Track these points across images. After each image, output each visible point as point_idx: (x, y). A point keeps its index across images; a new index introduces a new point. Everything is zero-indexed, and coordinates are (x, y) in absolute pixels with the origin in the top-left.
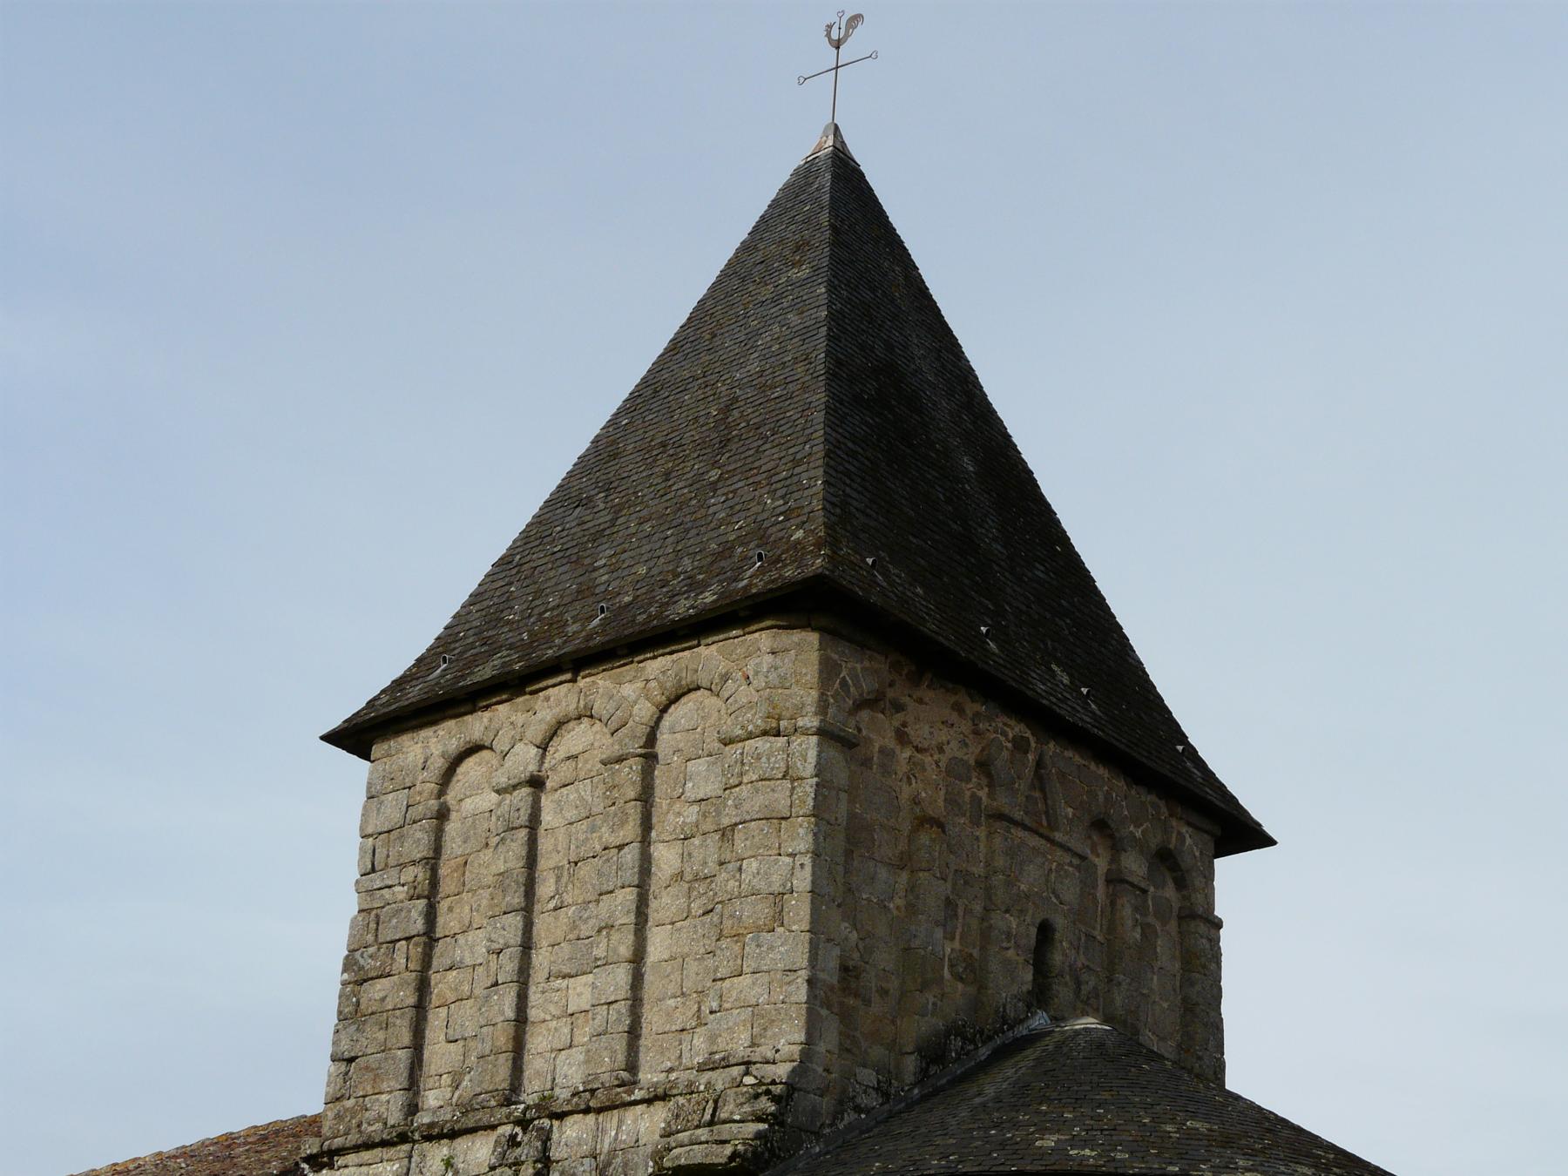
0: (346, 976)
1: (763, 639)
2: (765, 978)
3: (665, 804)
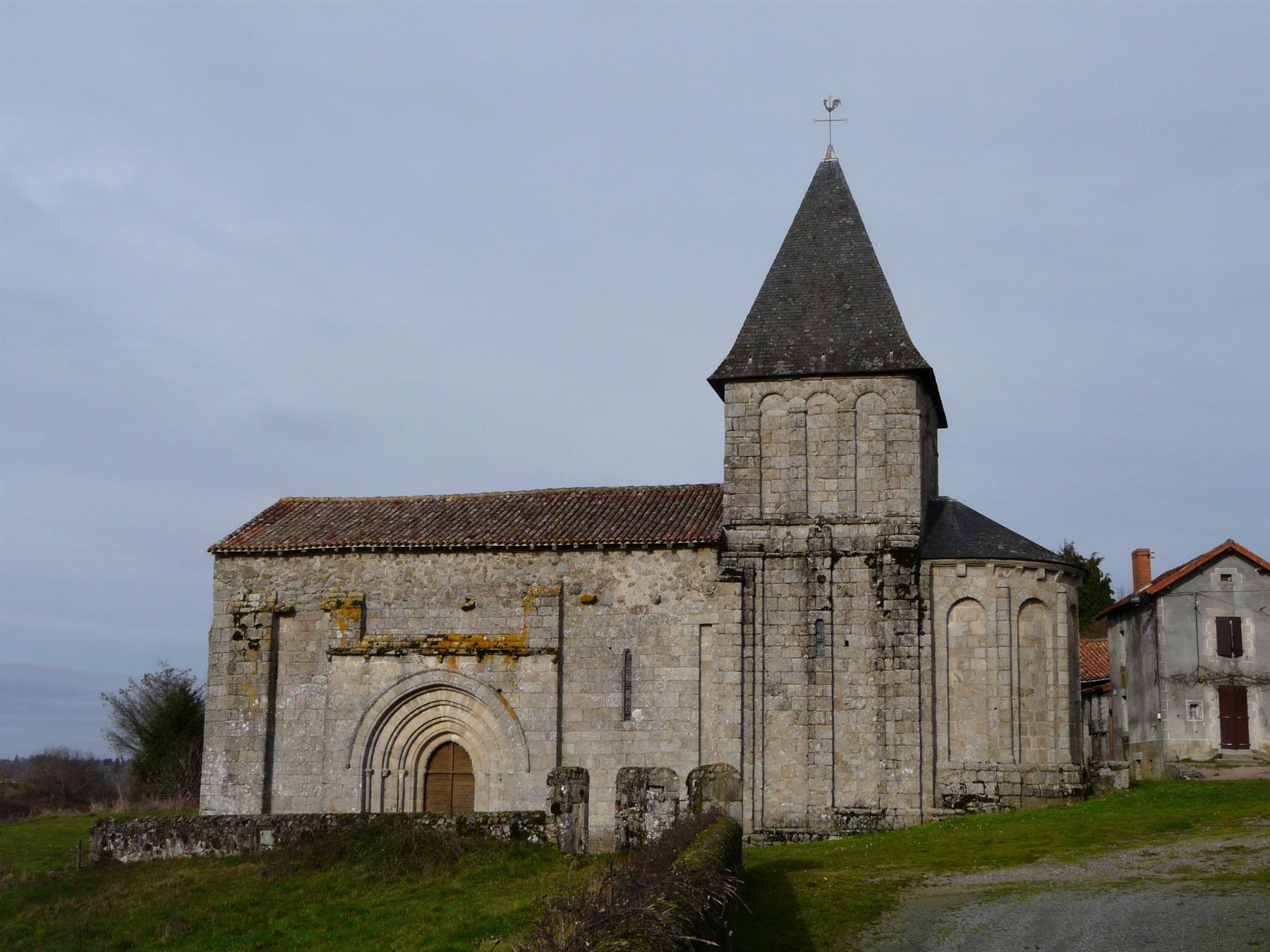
0: (726, 465)
1: (899, 381)
2: (908, 491)
3: (861, 428)
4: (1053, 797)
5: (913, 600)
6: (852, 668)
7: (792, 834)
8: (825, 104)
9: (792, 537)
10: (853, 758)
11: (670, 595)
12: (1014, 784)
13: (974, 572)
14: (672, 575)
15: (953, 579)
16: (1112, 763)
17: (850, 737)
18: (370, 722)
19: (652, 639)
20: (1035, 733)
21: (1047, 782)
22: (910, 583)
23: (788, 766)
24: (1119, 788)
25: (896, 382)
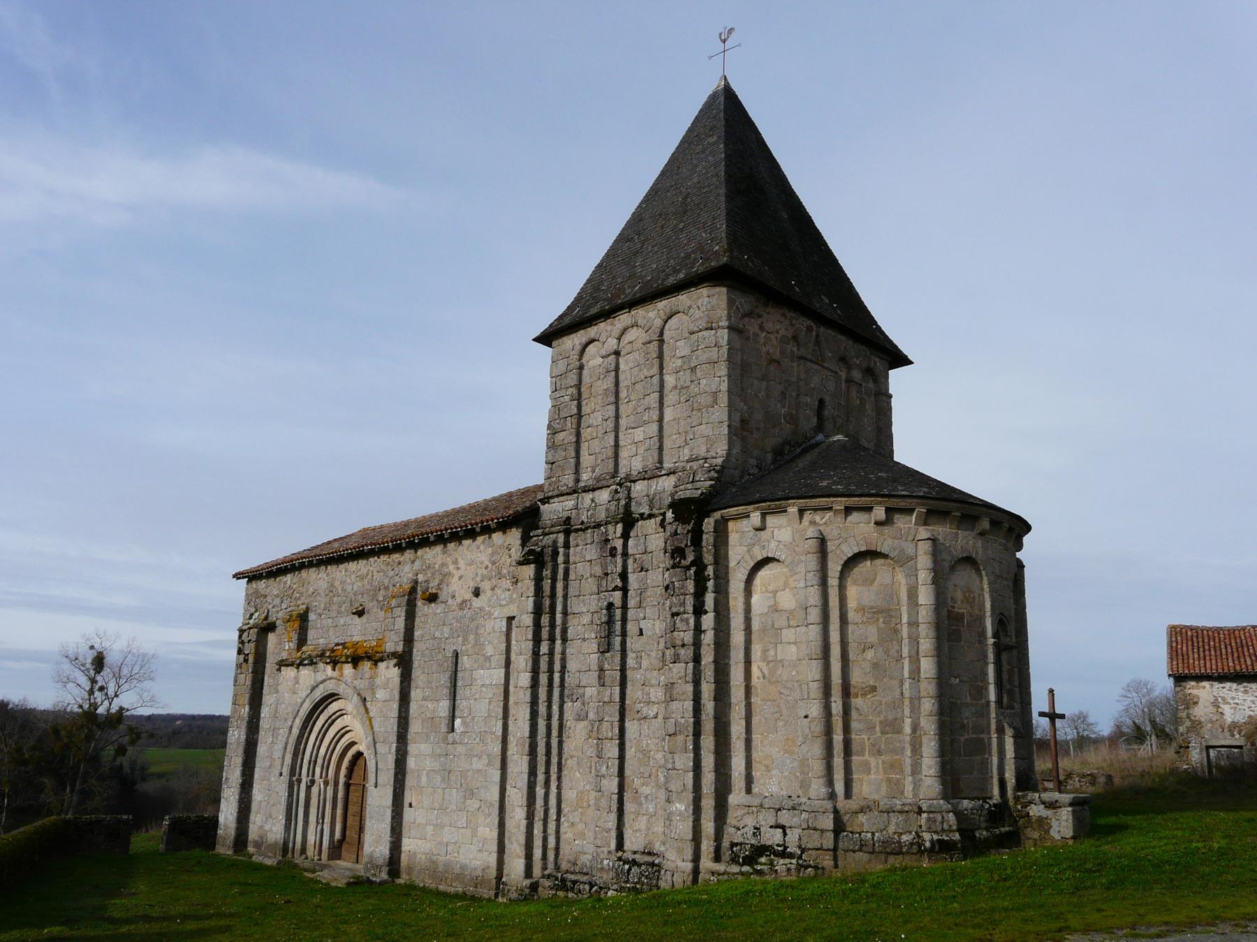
1: (704, 291)
3: (668, 359)
4: (900, 853)
5: (688, 568)
6: (645, 663)
7: (575, 882)
8: (720, 37)
9: (596, 503)
10: (643, 785)
11: (485, 586)
12: (823, 831)
13: (775, 521)
14: (487, 563)
15: (751, 534)
16: (1046, 796)
17: (641, 757)
18: (296, 731)
19: (471, 638)
20: (879, 752)
21: (892, 829)
22: (686, 545)
23: (581, 792)
24: (1057, 837)
25: (701, 292)
